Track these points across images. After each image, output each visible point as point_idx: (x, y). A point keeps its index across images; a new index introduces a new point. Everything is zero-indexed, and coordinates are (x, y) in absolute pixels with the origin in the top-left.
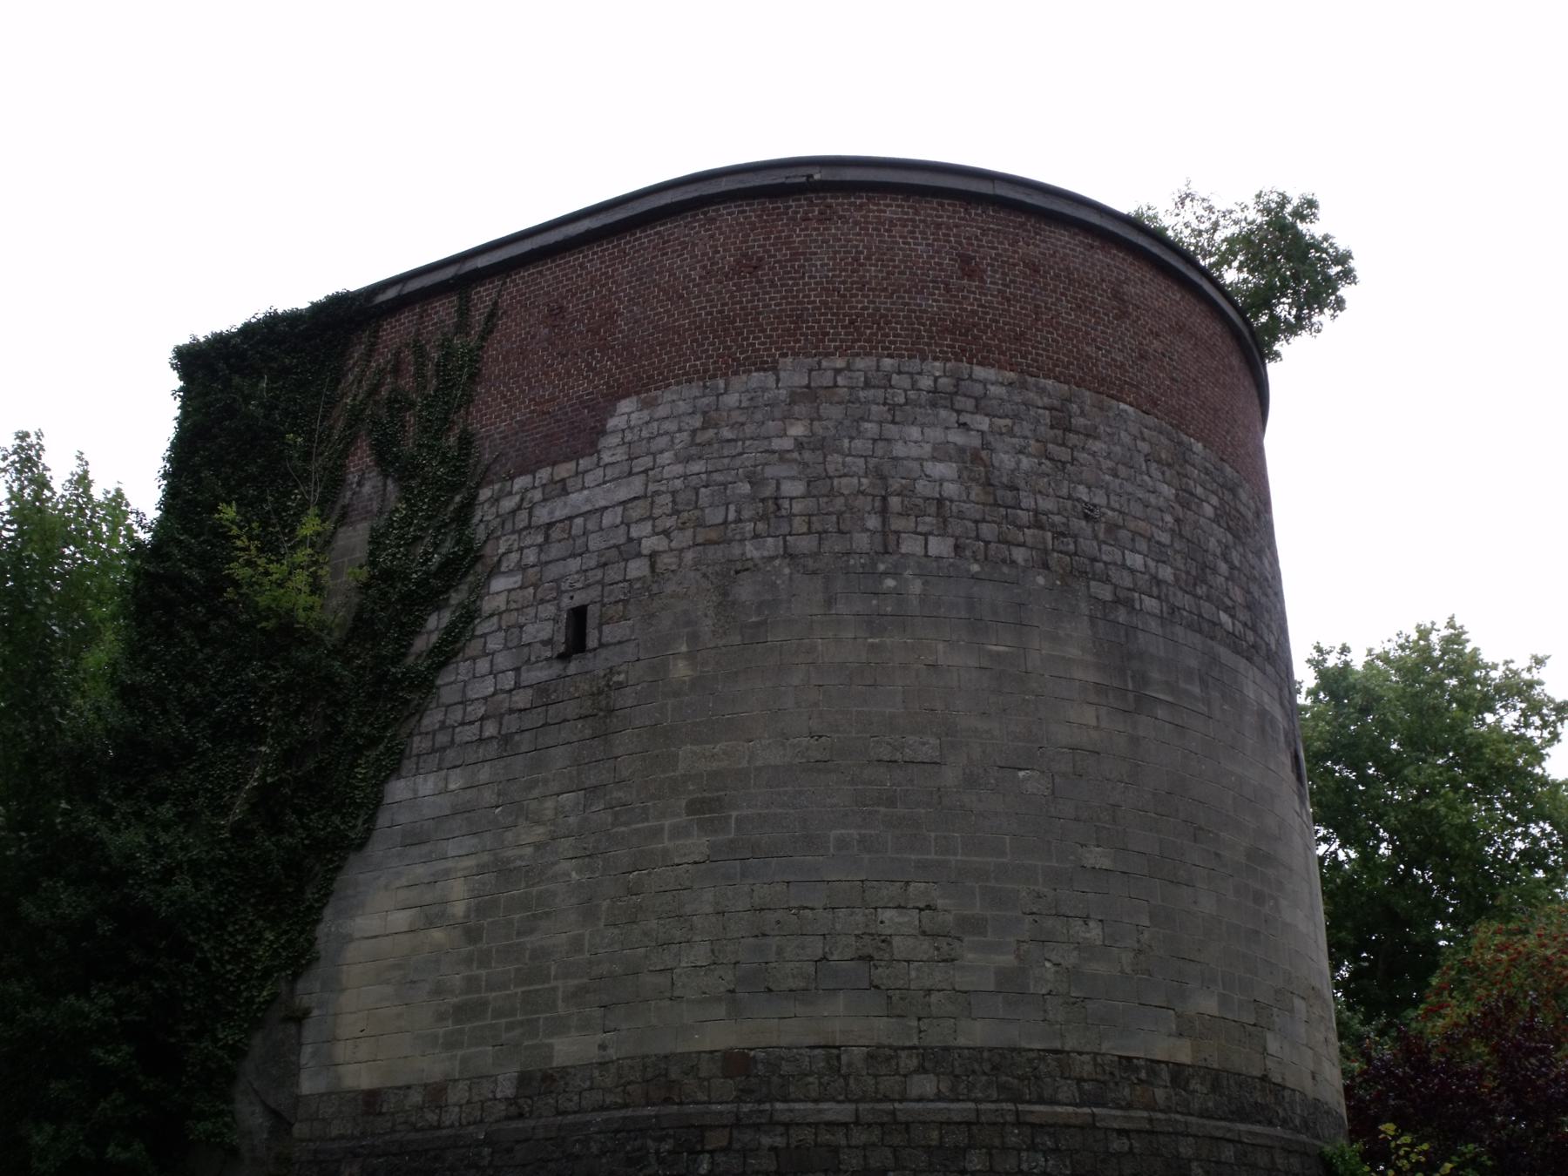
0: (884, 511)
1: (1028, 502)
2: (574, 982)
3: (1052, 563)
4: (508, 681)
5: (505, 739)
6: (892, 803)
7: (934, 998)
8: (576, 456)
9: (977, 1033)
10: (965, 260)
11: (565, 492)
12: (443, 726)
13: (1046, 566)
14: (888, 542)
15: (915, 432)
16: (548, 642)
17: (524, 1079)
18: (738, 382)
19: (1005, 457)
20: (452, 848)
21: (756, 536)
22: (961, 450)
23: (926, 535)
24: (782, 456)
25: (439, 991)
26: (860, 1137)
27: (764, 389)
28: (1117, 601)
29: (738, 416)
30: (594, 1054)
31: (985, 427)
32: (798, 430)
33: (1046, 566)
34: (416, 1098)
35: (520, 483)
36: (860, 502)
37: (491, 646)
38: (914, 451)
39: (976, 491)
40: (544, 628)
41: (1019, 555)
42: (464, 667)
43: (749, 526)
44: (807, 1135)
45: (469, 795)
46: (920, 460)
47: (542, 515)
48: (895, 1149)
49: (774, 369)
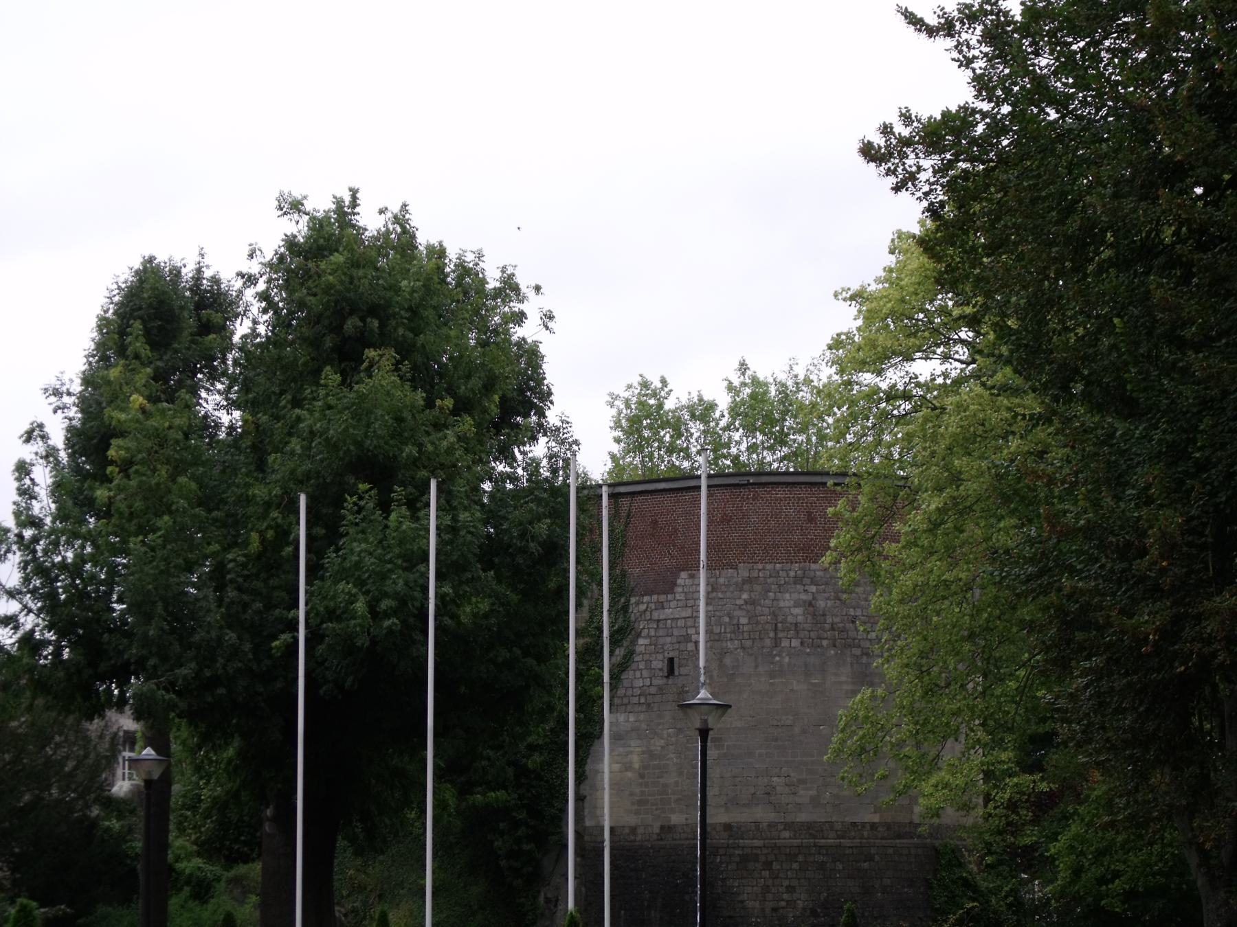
0: (776, 630)
1: (829, 620)
2: (676, 797)
3: (837, 644)
4: (648, 682)
5: (649, 705)
6: (776, 740)
7: (789, 806)
8: (666, 593)
9: (803, 817)
10: (809, 513)
11: (663, 608)
12: (625, 696)
13: (835, 646)
14: (777, 642)
15: (787, 596)
16: (661, 670)
17: (662, 827)
18: (724, 572)
19: (821, 602)
20: (633, 743)
21: (731, 639)
22: (805, 602)
23: (790, 638)
24: (740, 607)
25: (632, 794)
26: (765, 851)
27: (733, 577)
28: (863, 654)
29: (723, 588)
30: (683, 821)
31: (814, 590)
32: (745, 596)
33: (835, 646)
34: (627, 831)
35: (646, 599)
36: (767, 626)
37: (641, 667)
38: (787, 604)
39: (810, 618)
40: (659, 664)
41: (825, 643)
42: (631, 673)
43: (729, 635)
44: (749, 850)
45: (637, 724)
46: (789, 608)
47: (655, 615)
48: (776, 855)
49: (736, 568)
